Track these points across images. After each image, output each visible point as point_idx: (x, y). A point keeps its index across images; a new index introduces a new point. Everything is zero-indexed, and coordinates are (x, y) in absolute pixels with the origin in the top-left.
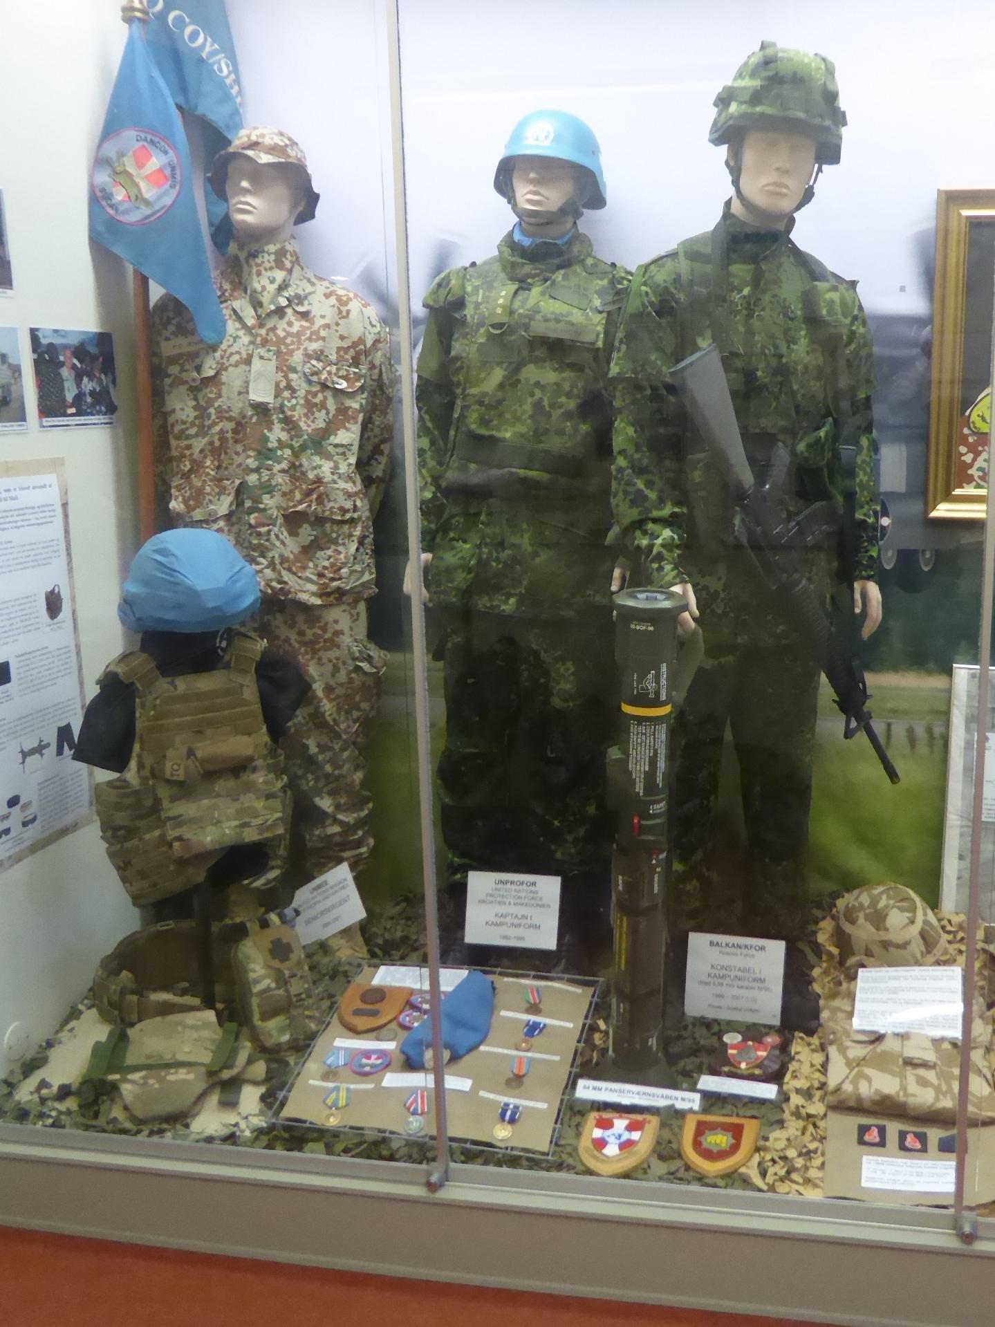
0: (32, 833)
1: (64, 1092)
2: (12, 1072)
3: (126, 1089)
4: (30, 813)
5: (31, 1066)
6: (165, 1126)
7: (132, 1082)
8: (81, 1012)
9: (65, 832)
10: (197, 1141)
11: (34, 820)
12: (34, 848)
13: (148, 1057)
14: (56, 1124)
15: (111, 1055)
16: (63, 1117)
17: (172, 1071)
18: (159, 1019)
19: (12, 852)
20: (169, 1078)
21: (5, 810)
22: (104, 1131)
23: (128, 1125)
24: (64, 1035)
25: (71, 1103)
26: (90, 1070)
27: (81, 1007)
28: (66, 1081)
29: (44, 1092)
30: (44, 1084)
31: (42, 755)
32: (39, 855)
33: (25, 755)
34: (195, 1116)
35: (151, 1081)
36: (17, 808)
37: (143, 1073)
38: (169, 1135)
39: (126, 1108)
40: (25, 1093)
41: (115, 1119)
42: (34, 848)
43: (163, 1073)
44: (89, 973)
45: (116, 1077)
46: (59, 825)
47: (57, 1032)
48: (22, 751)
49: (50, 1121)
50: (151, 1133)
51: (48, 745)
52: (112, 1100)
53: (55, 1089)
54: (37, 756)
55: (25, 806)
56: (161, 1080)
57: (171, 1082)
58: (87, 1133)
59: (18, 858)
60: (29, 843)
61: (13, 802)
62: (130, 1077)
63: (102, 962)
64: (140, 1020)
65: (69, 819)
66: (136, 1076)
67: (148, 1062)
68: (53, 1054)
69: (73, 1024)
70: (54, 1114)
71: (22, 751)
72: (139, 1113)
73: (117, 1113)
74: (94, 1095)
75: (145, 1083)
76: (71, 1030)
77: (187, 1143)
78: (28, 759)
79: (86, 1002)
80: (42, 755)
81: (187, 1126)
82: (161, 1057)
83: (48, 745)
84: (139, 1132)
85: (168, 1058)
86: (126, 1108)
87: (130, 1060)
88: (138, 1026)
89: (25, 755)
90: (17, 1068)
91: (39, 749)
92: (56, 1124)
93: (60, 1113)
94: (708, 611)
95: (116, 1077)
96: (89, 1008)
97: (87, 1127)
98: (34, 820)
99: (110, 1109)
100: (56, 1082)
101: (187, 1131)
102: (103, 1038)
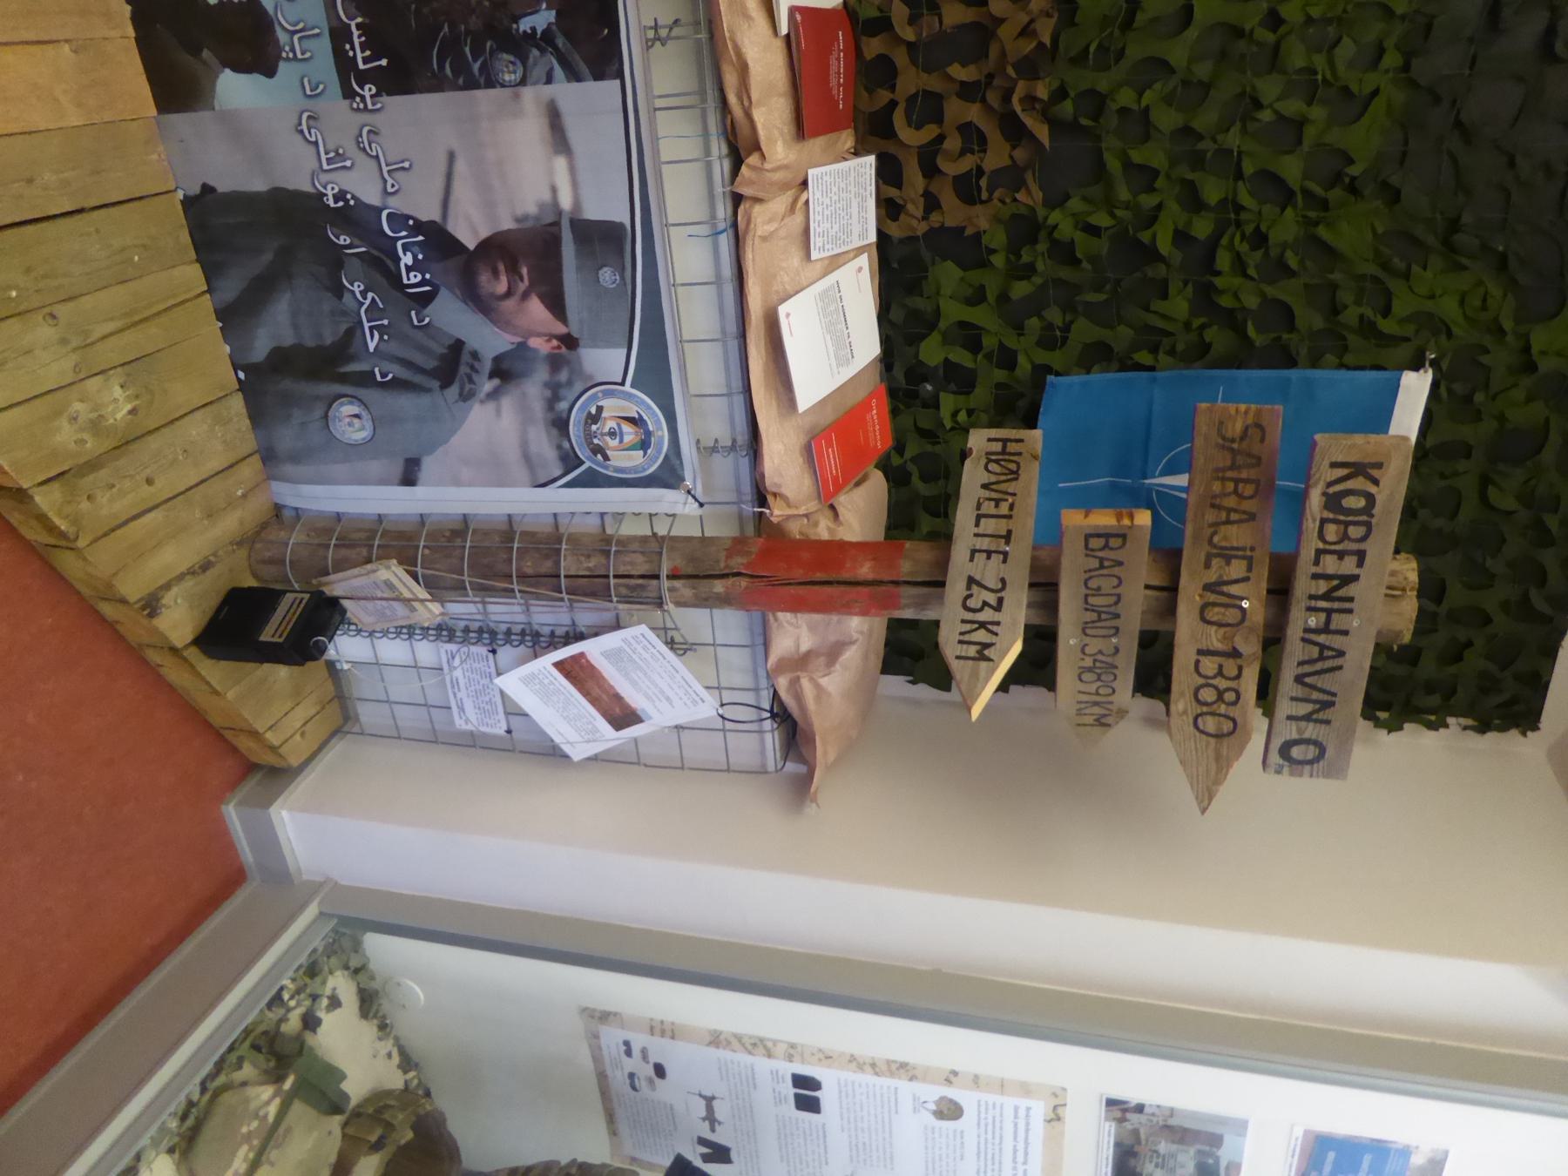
0: (618, 1079)
1: (310, 1022)
2: (372, 978)
3: (266, 1092)
4: (642, 1084)
5: (368, 1002)
6: (190, 1122)
7: (268, 1103)
8: (405, 1072)
9: (610, 1118)
10: (138, 1158)
11: (634, 1088)
12: (602, 1076)
13: (289, 1130)
14: (277, 1000)
15: (321, 1091)
16: (282, 1011)
17: (251, 1155)
18: (333, 1158)
19: (605, 1052)
20: (245, 1148)
21: (653, 1059)
22: (231, 1049)
23: (221, 1079)
24: (388, 1045)
25: (293, 1023)
26: (316, 1058)
27: (412, 1074)
28: (321, 1030)
29: (325, 1002)
30: (335, 1003)
31: (704, 1119)
32: (593, 1081)
33: (709, 1100)
34: (178, 1165)
35: (255, 1124)
36: (651, 1072)
37: (271, 1119)
38: (173, 1124)
39: (244, 1084)
40: (340, 983)
41: (240, 1067)
42: (602, 1076)
43: (256, 1142)
44: (444, 1102)
45: (288, 1084)
46: (620, 1113)
47: (397, 1039)
48: (713, 1098)
49: (286, 996)
50: (191, 1104)
51: (713, 1130)
52: (266, 1072)
53: (321, 1014)
54: (703, 1114)
55: (651, 1081)
56: (248, 1138)
57: (240, 1145)
58: (242, 1027)
59: (597, 1058)
60: (609, 1072)
61: (660, 1071)
62: (277, 1101)
63: (442, 1114)
64: (344, 1135)
65: (623, 1128)
66: (272, 1110)
67: (281, 1130)
68: (369, 1029)
69: (396, 1059)
70: (292, 1003)
71: (713, 1098)
72: (227, 1098)
73: (248, 1071)
74: (280, 1051)
75: (256, 1116)
76: (389, 1055)
77: (145, 1141)
78: (703, 1103)
79: (416, 1082)
80: (704, 1119)
81: (171, 1151)
82: (278, 1147)
83: (713, 1130)
84: (204, 1089)
85: (273, 1154)
86: (244, 1084)
87: (298, 1107)
88: (337, 1132)
89: (709, 1100)
90: (375, 985)
91: (711, 1118)
92: (277, 1000)
93: (289, 1010)
94: (1331, 30)
95: (288, 1084)
96: (406, 1082)
97: (247, 1032)
98: (634, 1088)
99: (255, 1066)
100: (329, 1020)
101: (165, 1144)
102: (346, 1086)
